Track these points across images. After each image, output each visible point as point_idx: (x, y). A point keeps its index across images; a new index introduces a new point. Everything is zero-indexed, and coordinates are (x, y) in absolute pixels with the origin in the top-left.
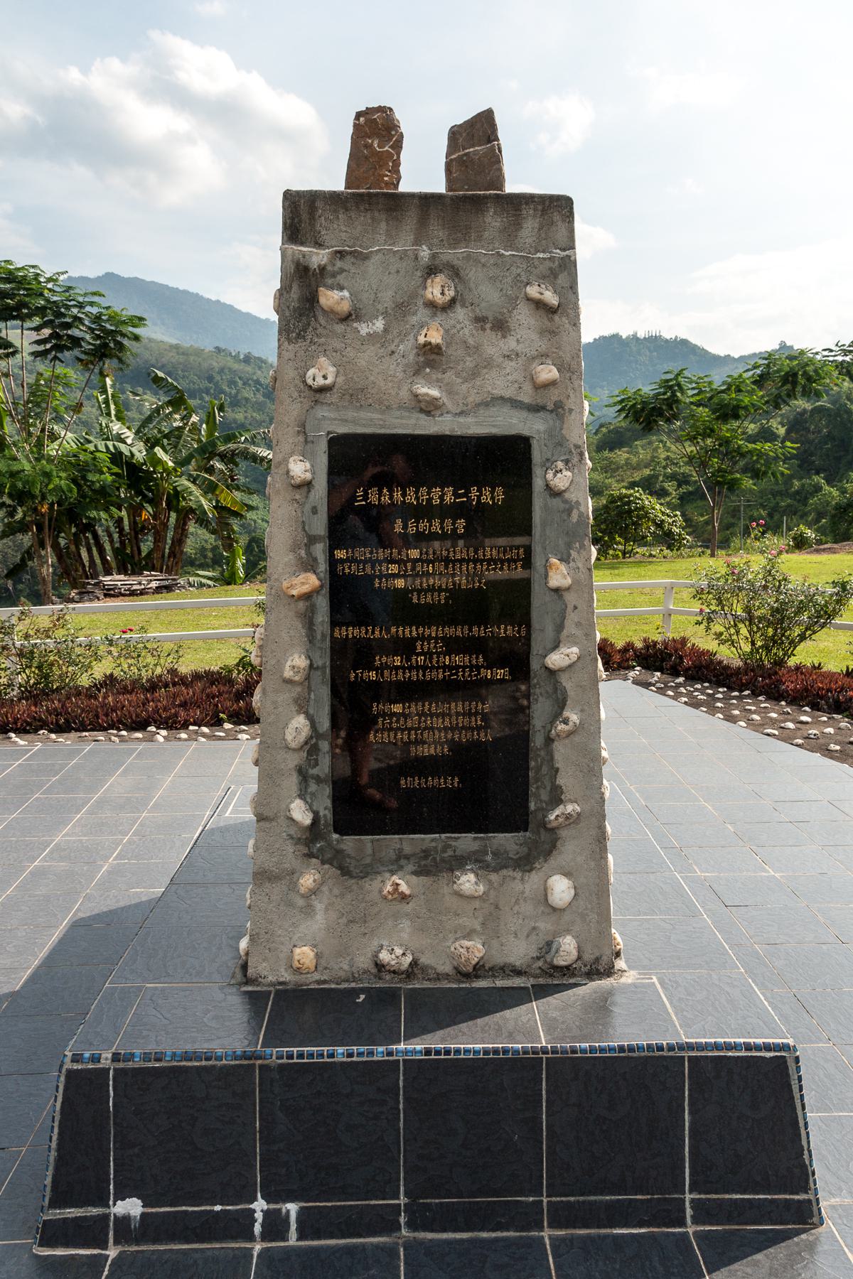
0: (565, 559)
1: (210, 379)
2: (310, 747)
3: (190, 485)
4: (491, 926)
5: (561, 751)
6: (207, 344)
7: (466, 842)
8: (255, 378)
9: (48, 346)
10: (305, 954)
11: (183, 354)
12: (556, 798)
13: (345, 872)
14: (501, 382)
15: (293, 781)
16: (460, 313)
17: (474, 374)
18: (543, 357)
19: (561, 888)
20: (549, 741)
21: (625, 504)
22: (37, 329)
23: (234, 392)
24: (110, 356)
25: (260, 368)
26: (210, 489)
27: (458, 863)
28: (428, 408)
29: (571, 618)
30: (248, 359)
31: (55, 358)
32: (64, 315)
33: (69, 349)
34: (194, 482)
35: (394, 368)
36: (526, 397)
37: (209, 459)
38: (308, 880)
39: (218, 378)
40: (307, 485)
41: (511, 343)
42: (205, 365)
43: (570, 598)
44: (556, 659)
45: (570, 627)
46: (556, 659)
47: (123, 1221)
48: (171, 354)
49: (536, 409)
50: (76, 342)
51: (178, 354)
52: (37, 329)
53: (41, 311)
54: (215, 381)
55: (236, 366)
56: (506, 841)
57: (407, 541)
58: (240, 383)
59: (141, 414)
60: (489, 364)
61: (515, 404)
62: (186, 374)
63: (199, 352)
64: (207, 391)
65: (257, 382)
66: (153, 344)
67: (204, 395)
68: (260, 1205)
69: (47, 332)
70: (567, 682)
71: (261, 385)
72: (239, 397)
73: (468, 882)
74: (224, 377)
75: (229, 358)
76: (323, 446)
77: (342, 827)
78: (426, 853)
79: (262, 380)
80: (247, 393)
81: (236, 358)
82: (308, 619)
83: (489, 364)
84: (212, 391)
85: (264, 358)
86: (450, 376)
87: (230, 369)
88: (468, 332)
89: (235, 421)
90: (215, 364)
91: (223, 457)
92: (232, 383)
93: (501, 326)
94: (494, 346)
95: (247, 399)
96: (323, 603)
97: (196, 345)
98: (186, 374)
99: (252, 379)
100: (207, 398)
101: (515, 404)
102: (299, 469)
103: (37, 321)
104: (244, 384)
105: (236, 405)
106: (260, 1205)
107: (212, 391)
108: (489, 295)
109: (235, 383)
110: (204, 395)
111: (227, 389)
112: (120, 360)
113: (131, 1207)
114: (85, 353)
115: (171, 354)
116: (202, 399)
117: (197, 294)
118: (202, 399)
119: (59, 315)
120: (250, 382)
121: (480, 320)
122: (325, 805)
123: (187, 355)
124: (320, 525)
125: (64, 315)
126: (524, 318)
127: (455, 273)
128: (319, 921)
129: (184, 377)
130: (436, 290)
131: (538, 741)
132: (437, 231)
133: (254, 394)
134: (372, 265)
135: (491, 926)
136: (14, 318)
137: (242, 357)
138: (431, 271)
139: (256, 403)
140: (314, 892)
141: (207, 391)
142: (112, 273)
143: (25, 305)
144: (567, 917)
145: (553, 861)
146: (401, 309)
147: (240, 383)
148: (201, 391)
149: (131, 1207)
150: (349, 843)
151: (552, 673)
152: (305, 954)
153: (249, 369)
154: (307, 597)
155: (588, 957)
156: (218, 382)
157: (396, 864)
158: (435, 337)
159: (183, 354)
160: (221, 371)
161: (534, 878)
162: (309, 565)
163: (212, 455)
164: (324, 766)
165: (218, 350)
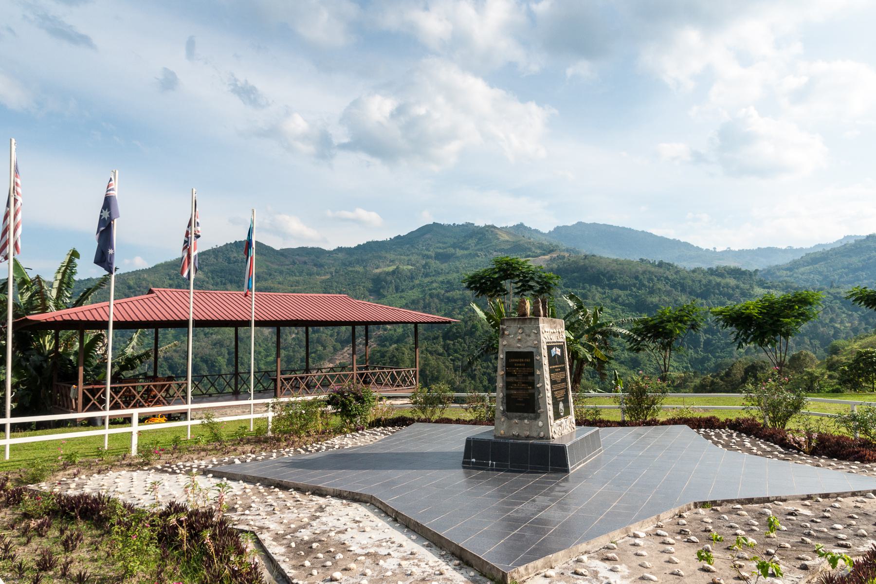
0: (539, 370)
1: (637, 278)
2: (503, 398)
3: (581, 347)
4: (530, 430)
5: (540, 401)
6: (635, 258)
7: (526, 415)
8: (665, 276)
9: (520, 290)
10: (502, 432)
11: (620, 264)
12: (539, 408)
13: (508, 419)
14: (529, 344)
15: (501, 403)
16: (523, 334)
17: (526, 342)
18: (535, 340)
19: (540, 424)
20: (538, 399)
21: (869, 357)
22: (516, 283)
23: (651, 285)
24: (545, 292)
25: (669, 269)
26: (591, 349)
27: (525, 418)
28: (519, 347)
29: (541, 379)
30: (661, 264)
31: (523, 294)
32: (527, 277)
33: (528, 290)
34: (583, 346)
35: (514, 342)
36: (533, 346)
37: (594, 335)
38: (503, 420)
39: (641, 277)
40: (502, 359)
41: (531, 338)
42: (634, 270)
43: (541, 376)
44: (538, 386)
45: (541, 381)
46: (538, 386)
47: (473, 462)
48: (613, 265)
49: (534, 347)
50: (531, 288)
51: (617, 264)
52: (516, 283)
53: (518, 276)
54: (640, 279)
55: (653, 269)
56: (532, 415)
57: (516, 367)
58: (655, 279)
59: (594, 301)
60: (528, 341)
61: (531, 347)
62: (622, 276)
63: (630, 263)
64: (634, 285)
65: (667, 278)
66: (602, 260)
67: (633, 288)
68: (490, 462)
69: (520, 284)
70: (540, 389)
71: (669, 280)
72: (655, 288)
73: (526, 421)
74: (645, 276)
75: (648, 265)
76: (505, 353)
77: (507, 411)
78: (520, 416)
79: (670, 277)
80: (660, 285)
81: (653, 264)
82: (503, 378)
83: (528, 341)
84: (637, 285)
85: (671, 263)
86: (522, 343)
87: (649, 272)
88: (525, 336)
89: (652, 303)
90: (640, 269)
91: (600, 333)
92: (650, 280)
93: (529, 336)
94: (528, 339)
95: (659, 289)
96: (505, 376)
97: (628, 259)
98: (622, 276)
99: (663, 277)
100: (634, 290)
101: (531, 347)
102: (501, 356)
103: (517, 279)
104: (658, 280)
105: (652, 293)
106: (490, 462)
107: (637, 285)
108: (527, 331)
109: (652, 280)
110: (633, 288)
111: (647, 283)
112: (549, 294)
113: (474, 460)
114: (535, 291)
115: (613, 265)
116: (631, 290)
117: (630, 229)
118: (631, 290)
119: (525, 277)
120: (662, 278)
121: (526, 335)
122: (505, 407)
123: (622, 264)
124: (504, 364)
125: (527, 277)
126: (532, 334)
127: (523, 328)
128: (505, 427)
129: (621, 277)
130: (520, 331)
131: (536, 398)
132: (520, 323)
133: (665, 286)
134: (512, 328)
135: (530, 430)
136: (508, 279)
137: (657, 263)
138: (520, 328)
139: (665, 291)
140: (504, 421)
141: (634, 285)
142: (581, 222)
143: (513, 274)
144: (542, 429)
145: (540, 419)
146: (516, 334)
147: (655, 279)
148: (630, 285)
149: (474, 460)
150: (508, 414)
151: (538, 388)
152: (502, 432)
153: (661, 270)
154: (502, 375)
155: (546, 436)
156: (641, 280)
157: (516, 418)
158: (520, 338)
159: (620, 264)
160: (644, 272)
161: (537, 422)
162: (503, 370)
163: (596, 333)
164: (505, 401)
165: (642, 260)
